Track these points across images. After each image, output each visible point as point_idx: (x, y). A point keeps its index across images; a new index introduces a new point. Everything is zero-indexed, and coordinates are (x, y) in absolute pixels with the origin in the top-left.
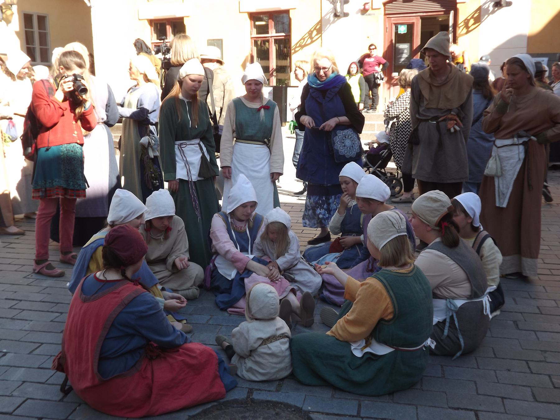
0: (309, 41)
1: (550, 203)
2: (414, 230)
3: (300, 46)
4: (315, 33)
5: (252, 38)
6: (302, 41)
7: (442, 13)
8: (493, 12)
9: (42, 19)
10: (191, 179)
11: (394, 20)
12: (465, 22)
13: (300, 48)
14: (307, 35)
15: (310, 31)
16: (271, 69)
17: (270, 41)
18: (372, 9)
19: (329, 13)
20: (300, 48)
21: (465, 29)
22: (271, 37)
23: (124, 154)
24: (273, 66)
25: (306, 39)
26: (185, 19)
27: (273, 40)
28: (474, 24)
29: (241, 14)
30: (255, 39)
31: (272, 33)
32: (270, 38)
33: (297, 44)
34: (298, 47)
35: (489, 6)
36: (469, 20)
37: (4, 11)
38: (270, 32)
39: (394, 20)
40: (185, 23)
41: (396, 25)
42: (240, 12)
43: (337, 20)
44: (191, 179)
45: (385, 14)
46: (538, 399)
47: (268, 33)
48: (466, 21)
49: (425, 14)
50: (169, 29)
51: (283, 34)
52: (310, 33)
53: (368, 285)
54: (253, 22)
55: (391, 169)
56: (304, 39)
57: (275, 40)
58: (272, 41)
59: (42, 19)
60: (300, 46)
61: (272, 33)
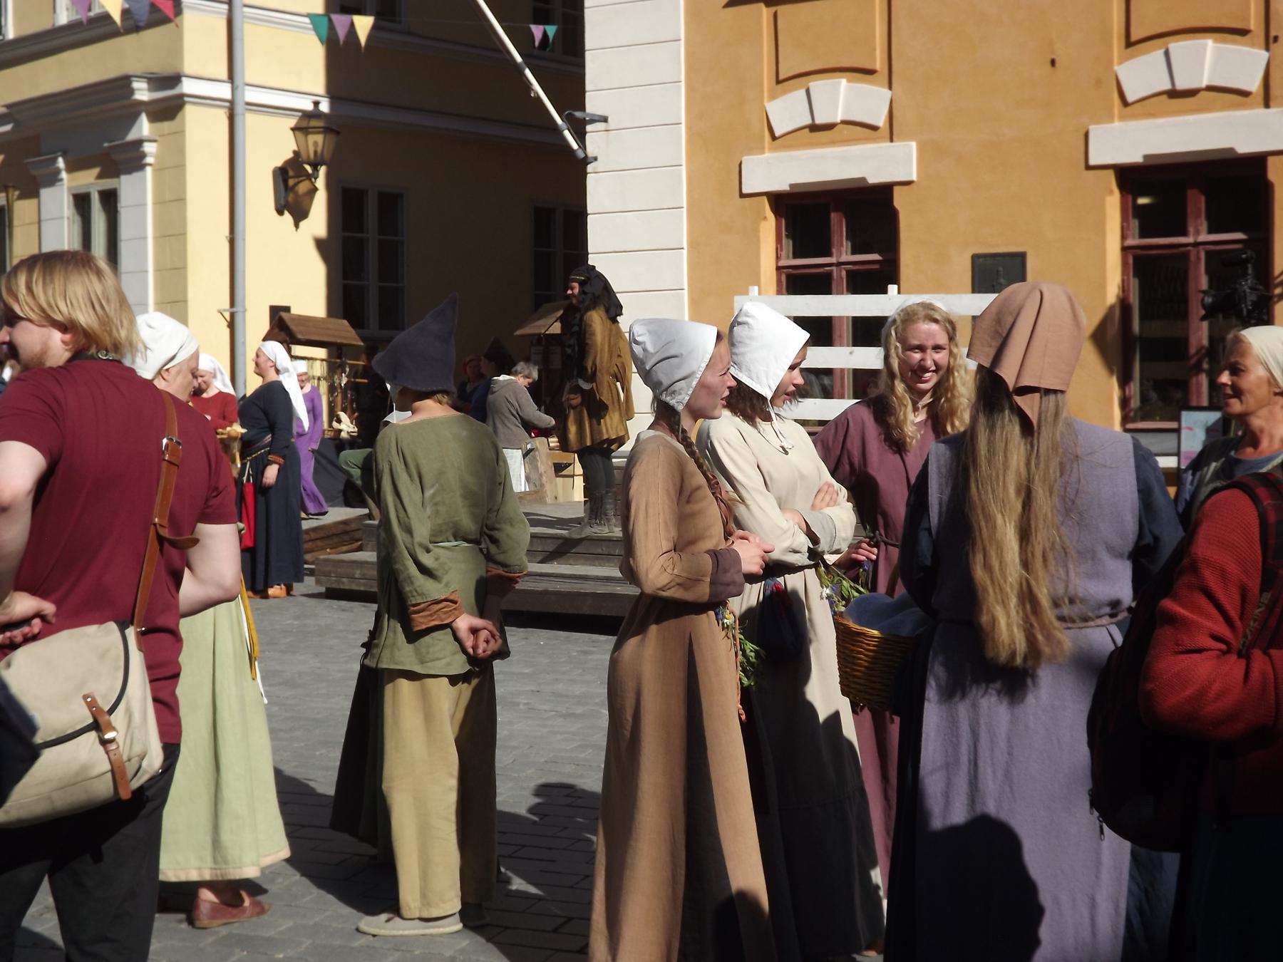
5: (778, 268)
9: (390, 203)
16: (1193, 350)
17: (1193, 257)
22: (839, 264)
24: (1200, 339)
27: (1203, 256)
29: (1091, 173)
30: (1139, 252)
31: (840, 255)
32: (1189, 248)
37: (291, 182)
38: (1191, 230)
40: (1272, 175)
42: (742, 196)
47: (829, 254)
50: (838, 225)
51: (876, 257)
53: (572, 790)
54: (1130, 198)
55: (321, 534)
57: (1208, 253)
58: (1198, 259)
59: (390, 203)
61: (1200, 234)
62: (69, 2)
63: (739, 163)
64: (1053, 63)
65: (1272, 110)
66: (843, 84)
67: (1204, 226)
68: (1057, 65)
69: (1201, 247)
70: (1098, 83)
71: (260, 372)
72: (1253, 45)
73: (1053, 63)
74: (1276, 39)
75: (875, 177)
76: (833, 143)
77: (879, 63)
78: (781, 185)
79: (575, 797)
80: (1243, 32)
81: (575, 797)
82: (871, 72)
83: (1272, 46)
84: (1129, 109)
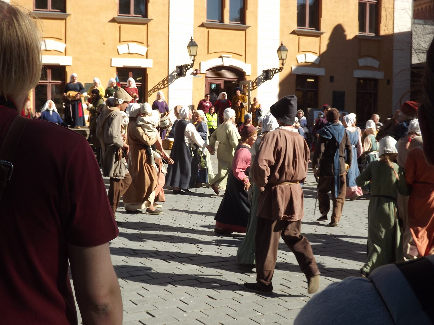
0: (163, 87)
1: (249, 196)
2: (103, 175)
3: (157, 88)
4: (166, 82)
6: (159, 85)
7: (237, 80)
8: (177, 78)
10: (338, 203)
11: (210, 81)
12: (162, 82)
13: (157, 90)
14: (161, 82)
15: (163, 80)
18: (200, 73)
19: (174, 72)
20: (157, 90)
21: (163, 85)
23: (318, 176)
25: (161, 85)
26: (148, 70)
28: (256, 86)
29: (112, 68)
31: (49, 80)
33: (155, 86)
34: (156, 89)
35: (262, 78)
36: (165, 81)
38: (48, 79)
39: (209, 81)
41: (211, 84)
43: (178, 78)
44: (338, 203)
45: (206, 77)
46: (146, 276)
47: (47, 80)
48: (163, 81)
49: (226, 79)
52: (163, 81)
56: (160, 84)
60: (157, 88)
62: (413, 0)
63: (199, 63)
64: (104, 44)
65: (67, 57)
66: (53, 41)
67: (50, 79)
68: (105, 44)
69: (51, 83)
70: (114, 49)
71: (177, 114)
72: (144, 46)
73: (104, 44)
74: (149, 46)
75: (143, 66)
76: (50, 54)
77: (63, 38)
78: (121, 66)
79: (198, 281)
80: (143, 43)
81: (198, 281)
82: (61, 39)
83: (148, 47)
84: (119, 55)
